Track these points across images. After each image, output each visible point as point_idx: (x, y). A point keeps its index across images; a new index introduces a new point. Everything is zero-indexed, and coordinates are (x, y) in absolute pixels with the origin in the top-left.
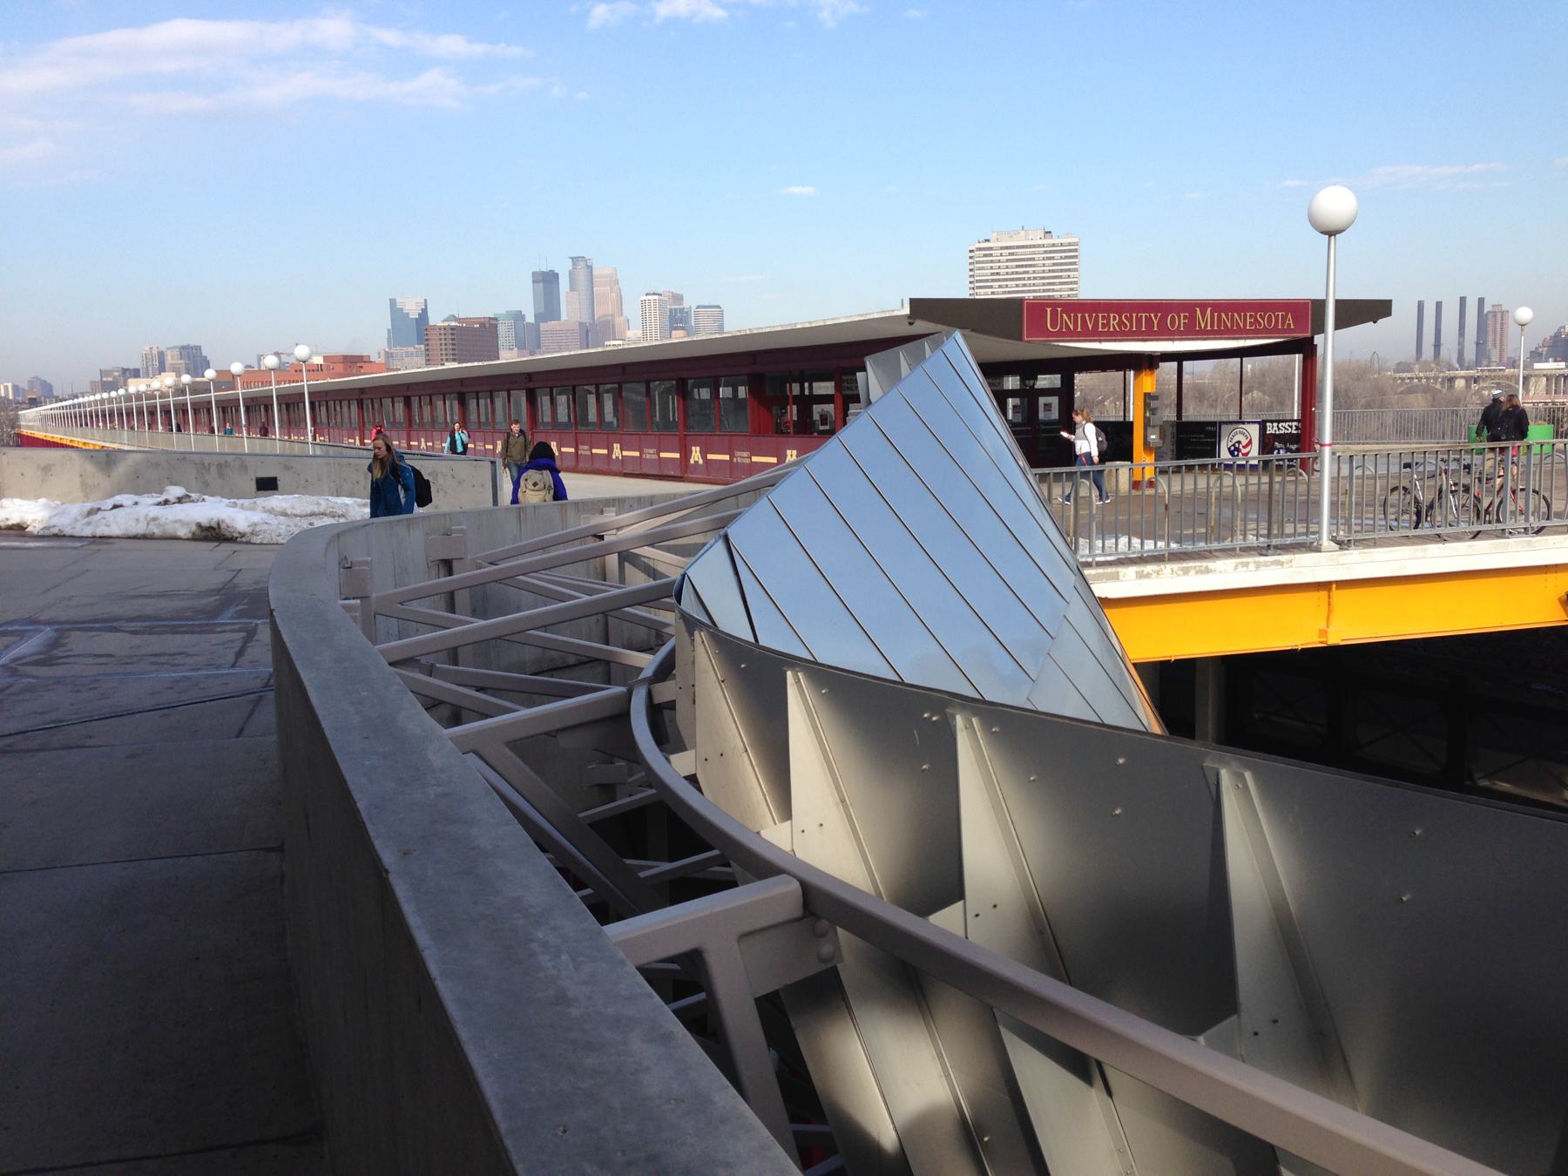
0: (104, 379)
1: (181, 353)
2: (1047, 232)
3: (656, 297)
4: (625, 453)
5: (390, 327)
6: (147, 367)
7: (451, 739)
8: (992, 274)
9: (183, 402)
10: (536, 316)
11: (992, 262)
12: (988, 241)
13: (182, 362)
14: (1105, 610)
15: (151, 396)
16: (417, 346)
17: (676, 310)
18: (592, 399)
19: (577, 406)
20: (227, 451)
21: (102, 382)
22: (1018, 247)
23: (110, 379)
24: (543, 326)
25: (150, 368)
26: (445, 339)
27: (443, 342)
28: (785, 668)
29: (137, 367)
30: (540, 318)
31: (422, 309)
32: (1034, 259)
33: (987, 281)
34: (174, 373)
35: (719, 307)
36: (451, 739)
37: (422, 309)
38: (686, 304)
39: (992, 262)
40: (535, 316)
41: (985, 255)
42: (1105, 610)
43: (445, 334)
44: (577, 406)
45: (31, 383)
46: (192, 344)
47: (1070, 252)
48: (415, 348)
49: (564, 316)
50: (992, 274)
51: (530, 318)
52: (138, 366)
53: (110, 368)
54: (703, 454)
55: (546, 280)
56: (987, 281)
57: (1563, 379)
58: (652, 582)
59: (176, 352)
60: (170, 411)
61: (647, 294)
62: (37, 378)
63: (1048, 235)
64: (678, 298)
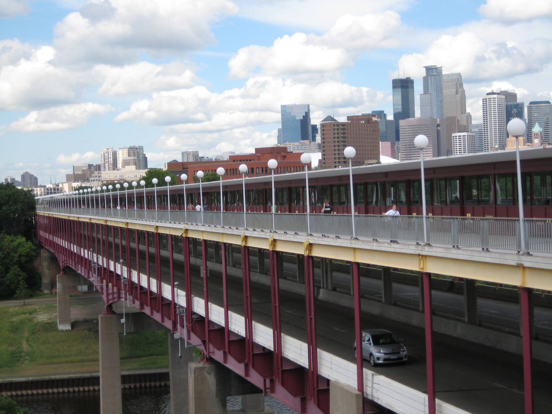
1: (129, 153)
6: (104, 164)
9: (97, 196)
14: (123, 266)
15: (53, 198)
16: (301, 141)
18: (47, 223)
20: (483, 185)
24: (402, 123)
25: (107, 165)
26: (338, 133)
27: (336, 132)
29: (99, 163)
30: (398, 116)
32: (43, 205)
34: (302, 118)
37: (306, 113)
42: (123, 266)
43: (338, 129)
46: (137, 146)
48: (300, 143)
49: (418, 113)
57: (490, 176)
58: (80, 273)
59: (126, 151)
60: (188, 184)
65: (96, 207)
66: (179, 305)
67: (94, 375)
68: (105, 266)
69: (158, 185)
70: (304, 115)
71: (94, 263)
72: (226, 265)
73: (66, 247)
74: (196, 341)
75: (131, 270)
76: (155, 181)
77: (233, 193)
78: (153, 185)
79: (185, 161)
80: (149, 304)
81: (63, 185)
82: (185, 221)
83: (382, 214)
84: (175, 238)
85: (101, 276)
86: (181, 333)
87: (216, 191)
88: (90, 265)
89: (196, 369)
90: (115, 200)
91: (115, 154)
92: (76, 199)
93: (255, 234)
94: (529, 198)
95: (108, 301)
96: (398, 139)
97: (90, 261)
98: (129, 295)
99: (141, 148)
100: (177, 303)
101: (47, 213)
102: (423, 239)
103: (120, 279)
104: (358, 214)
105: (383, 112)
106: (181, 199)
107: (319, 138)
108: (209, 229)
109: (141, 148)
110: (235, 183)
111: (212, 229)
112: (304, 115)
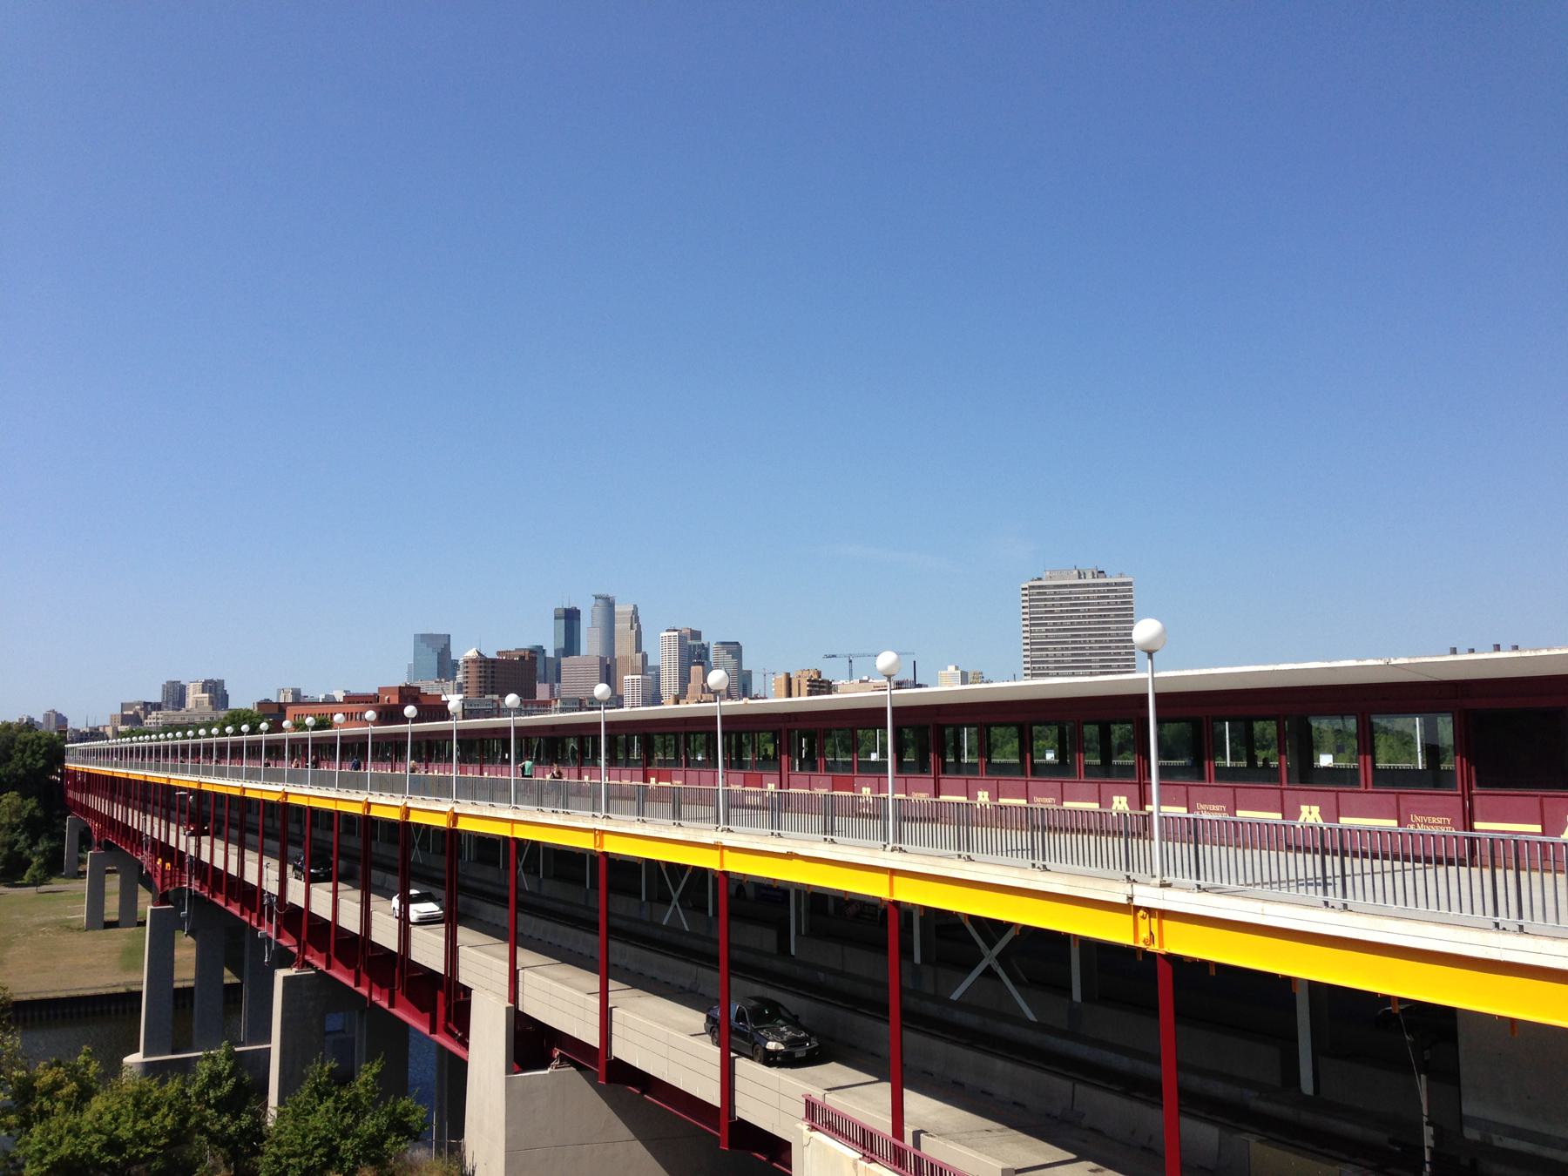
0: (125, 713)
2: (1099, 572)
3: (676, 633)
4: (661, 784)
5: (412, 662)
7: (37, 870)
8: (1046, 612)
10: (556, 651)
11: (1045, 600)
12: (1040, 579)
13: (207, 695)
17: (694, 646)
19: (1026, 747)
21: (123, 715)
22: (1116, 584)
23: (131, 713)
28: (442, 912)
31: (445, 645)
33: (1041, 618)
35: (737, 643)
36: (37, 870)
37: (445, 645)
38: (704, 640)
39: (1045, 600)
40: (555, 651)
41: (1039, 594)
44: (1026, 747)
45: (47, 716)
47: (409, 665)
50: (1046, 612)
51: (550, 654)
52: (159, 700)
53: (132, 701)
54: (657, 781)
55: (571, 617)
56: (1041, 618)
59: (199, 686)
61: (668, 631)
62: (53, 711)
63: (1102, 574)
64: (696, 635)
65: (130, 757)
66: (268, 893)
67: (134, 988)
68: (163, 840)
69: (250, 733)
70: (443, 647)
71: (147, 835)
72: (263, 817)
73: (120, 819)
74: (288, 942)
75: (512, 1005)
76: (245, 728)
77: (254, 748)
78: (241, 733)
79: (282, 701)
80: (224, 891)
81: (104, 729)
82: (404, 792)
83: (767, 787)
84: (349, 818)
85: (156, 854)
86: (268, 930)
87: (591, 733)
88: (141, 838)
89: (286, 979)
90: (131, 752)
91: (183, 689)
92: (112, 749)
93: (382, 800)
94: (953, 760)
95: (163, 887)
96: (559, 680)
97: (141, 833)
98: (195, 879)
99: (221, 683)
100: (265, 889)
101: (80, 767)
102: (600, 810)
103: (184, 859)
104: (775, 788)
105: (542, 647)
106: (1146, 761)
107: (460, 677)
108: (317, 793)
109: (221, 683)
110: (355, 734)
111: (323, 792)
112: (443, 647)
